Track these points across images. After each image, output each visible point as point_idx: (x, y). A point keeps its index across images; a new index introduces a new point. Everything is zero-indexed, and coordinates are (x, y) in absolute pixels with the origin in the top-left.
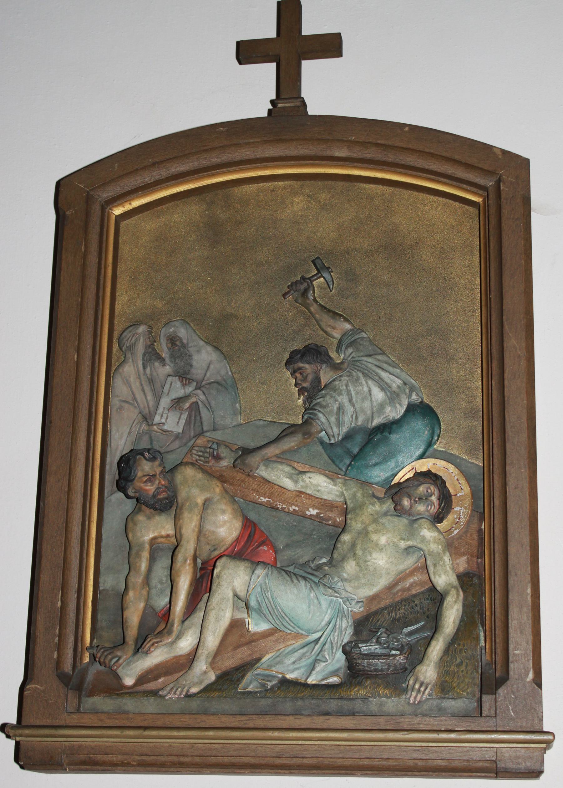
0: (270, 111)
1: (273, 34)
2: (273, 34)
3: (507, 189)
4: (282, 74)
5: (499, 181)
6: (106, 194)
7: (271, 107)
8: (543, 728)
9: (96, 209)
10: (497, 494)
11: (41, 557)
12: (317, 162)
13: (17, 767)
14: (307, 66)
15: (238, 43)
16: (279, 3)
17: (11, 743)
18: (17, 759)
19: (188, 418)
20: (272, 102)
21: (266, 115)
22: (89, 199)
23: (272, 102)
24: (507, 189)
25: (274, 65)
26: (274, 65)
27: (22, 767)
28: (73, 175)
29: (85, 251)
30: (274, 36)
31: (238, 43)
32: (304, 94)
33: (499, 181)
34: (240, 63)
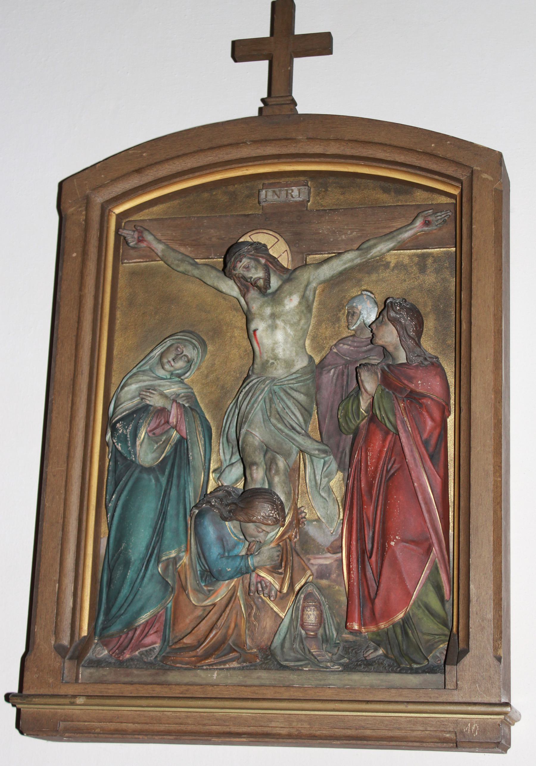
0: (260, 109)
2: (266, 33)
3: (381, 652)
4: (275, 73)
7: (262, 105)
8: (448, 665)
11: (36, 607)
12: (231, 654)
13: (17, 731)
15: (234, 43)
16: (273, 4)
17: (14, 710)
18: (18, 726)
20: (263, 100)
22: (87, 202)
23: (263, 100)
24: (381, 652)
28: (71, 178)
29: (43, 731)
30: (268, 35)
31: (234, 43)
32: (294, 95)
34: (236, 61)
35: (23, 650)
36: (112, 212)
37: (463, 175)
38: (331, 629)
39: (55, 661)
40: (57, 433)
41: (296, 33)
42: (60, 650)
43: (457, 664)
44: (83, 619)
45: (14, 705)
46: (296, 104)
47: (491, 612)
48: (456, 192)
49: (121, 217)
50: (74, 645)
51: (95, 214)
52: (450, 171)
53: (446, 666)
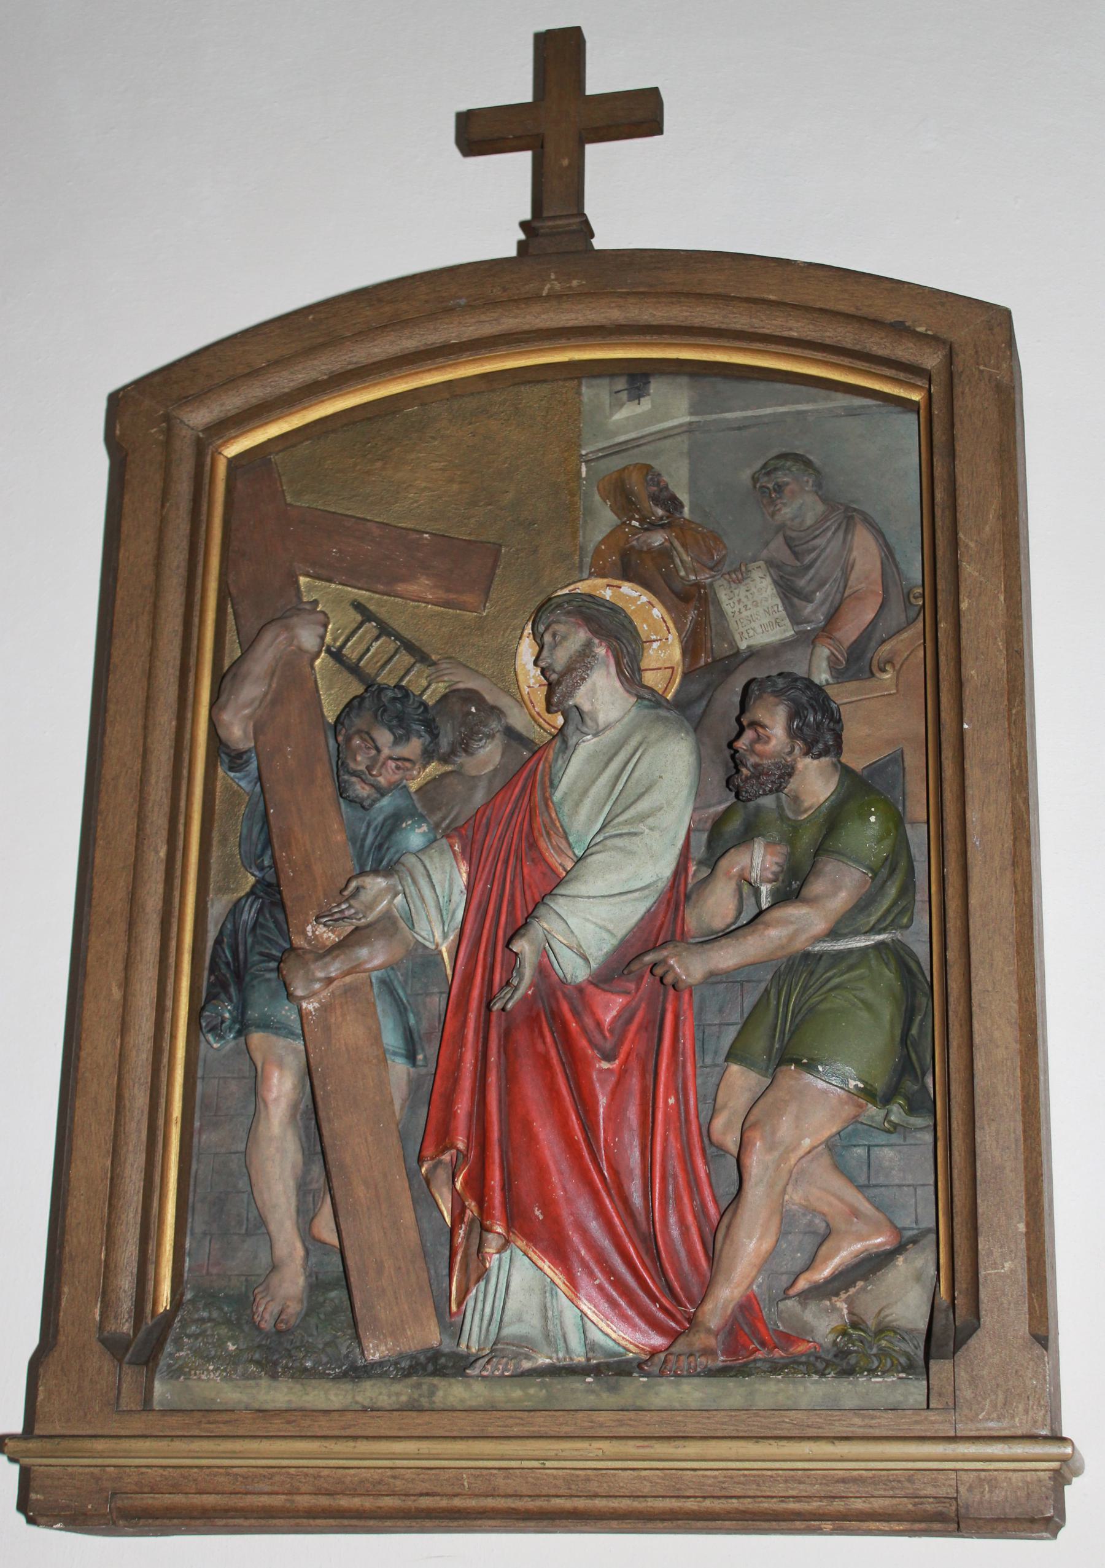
0: (521, 245)
1: (525, 95)
2: (525, 95)
5: (391, 758)
6: (199, 417)
7: (522, 236)
9: (185, 450)
10: (958, 1143)
13: (21, 1518)
14: (595, 153)
17: (15, 1469)
18: (23, 1505)
19: (503, 1057)
20: (524, 225)
21: (513, 253)
23: (524, 225)
25: (525, 158)
26: (525, 158)
27: (31, 1521)
33: (391, 758)
35: (32, 1340)
36: (220, 453)
37: (932, 360)
38: (680, 879)
39: (99, 1362)
40: (118, 751)
41: (588, 93)
42: (115, 1346)
43: (954, 1353)
44: (168, 1183)
45: (12, 1460)
46: (592, 235)
47: (1024, 1303)
48: (916, 397)
49: (234, 463)
50: (140, 1335)
51: (185, 450)
52: (905, 351)
53: (932, 1362)
